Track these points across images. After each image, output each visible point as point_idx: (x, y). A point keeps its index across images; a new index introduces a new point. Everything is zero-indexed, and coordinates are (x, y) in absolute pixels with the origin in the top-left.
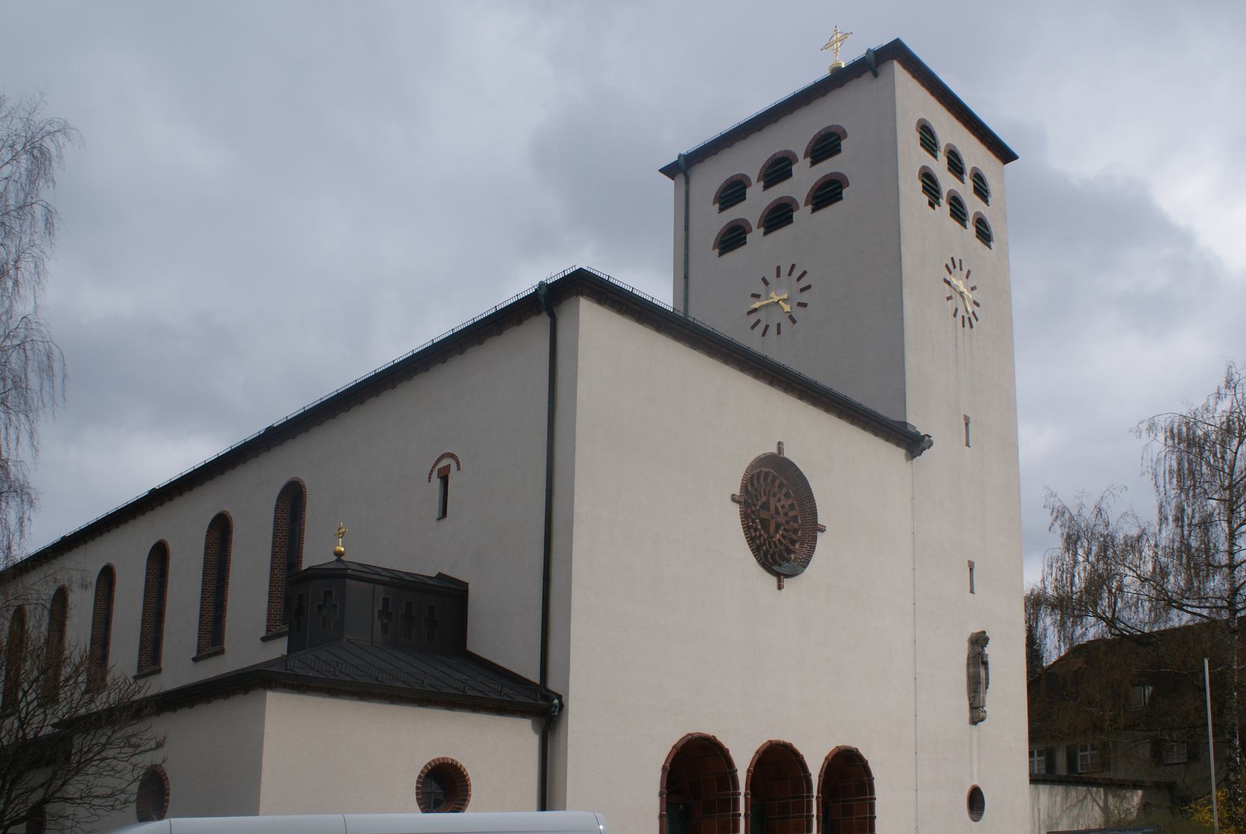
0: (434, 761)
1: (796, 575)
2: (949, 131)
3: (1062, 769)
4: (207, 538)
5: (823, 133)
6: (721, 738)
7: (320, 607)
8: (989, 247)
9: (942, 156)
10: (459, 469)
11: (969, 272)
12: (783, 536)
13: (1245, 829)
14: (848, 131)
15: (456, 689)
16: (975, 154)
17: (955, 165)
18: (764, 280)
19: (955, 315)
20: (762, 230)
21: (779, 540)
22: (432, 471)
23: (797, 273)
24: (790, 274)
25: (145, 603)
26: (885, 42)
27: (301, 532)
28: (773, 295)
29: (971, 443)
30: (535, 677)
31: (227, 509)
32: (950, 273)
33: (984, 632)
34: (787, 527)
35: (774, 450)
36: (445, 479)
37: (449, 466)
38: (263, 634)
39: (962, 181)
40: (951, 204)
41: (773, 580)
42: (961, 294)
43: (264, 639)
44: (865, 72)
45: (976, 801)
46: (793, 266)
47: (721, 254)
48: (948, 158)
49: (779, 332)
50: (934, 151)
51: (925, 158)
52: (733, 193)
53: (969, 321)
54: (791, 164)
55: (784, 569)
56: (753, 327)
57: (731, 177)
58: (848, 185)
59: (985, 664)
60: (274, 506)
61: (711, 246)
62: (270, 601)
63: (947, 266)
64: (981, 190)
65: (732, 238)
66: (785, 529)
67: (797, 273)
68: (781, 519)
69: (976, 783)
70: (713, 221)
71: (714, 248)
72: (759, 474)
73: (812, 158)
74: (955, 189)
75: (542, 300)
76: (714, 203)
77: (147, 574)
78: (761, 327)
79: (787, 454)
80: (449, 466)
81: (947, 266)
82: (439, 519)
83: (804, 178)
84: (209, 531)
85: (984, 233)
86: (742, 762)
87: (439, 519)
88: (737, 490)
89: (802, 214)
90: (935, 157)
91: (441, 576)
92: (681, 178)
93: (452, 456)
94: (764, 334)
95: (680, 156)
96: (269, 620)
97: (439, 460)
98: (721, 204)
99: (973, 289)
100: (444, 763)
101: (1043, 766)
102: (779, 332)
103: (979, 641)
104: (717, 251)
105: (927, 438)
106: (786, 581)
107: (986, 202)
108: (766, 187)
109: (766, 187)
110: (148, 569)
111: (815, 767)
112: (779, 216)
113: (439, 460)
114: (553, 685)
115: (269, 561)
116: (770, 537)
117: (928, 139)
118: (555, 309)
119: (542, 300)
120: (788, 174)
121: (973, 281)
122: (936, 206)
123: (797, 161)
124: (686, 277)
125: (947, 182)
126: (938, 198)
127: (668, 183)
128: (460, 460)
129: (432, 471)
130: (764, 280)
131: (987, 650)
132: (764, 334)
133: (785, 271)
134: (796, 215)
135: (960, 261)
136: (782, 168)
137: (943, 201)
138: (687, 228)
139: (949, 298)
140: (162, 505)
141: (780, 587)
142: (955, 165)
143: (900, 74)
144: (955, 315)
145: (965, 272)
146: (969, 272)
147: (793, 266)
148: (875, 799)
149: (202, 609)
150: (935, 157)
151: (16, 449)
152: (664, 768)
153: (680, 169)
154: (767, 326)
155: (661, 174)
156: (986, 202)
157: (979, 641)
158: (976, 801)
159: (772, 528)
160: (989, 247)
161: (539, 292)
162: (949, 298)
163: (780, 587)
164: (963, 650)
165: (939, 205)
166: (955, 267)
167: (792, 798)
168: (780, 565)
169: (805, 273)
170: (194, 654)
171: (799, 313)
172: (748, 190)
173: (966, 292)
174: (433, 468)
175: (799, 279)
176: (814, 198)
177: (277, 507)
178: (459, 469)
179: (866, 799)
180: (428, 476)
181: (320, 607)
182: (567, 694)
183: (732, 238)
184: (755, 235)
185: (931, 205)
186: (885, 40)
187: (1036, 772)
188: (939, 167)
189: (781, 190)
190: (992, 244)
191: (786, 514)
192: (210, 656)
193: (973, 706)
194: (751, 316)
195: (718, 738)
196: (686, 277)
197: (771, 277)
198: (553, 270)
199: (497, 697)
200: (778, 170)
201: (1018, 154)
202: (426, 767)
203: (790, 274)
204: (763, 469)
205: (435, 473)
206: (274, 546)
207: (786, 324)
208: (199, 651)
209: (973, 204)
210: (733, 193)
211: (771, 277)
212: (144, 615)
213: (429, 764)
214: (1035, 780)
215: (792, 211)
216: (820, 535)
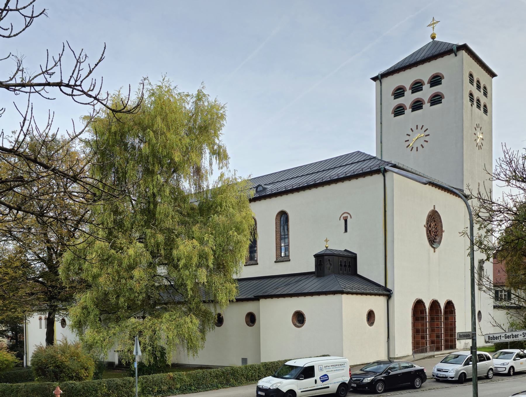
13: (59, 396)
16: (479, 74)
18: (411, 129)
20: (411, 110)
22: (341, 217)
23: (424, 129)
24: (421, 129)
36: (346, 221)
46: (423, 126)
50: (472, 82)
52: (399, 92)
54: (422, 85)
57: (416, 80)
65: (399, 111)
67: (424, 129)
71: (392, 113)
73: (431, 84)
83: (427, 93)
89: (427, 105)
91: (346, 250)
92: (378, 81)
97: (343, 214)
104: (393, 115)
108: (413, 93)
109: (413, 93)
112: (417, 105)
113: (343, 214)
114: (389, 287)
127: (374, 83)
129: (341, 217)
130: (411, 129)
143: (463, 53)
147: (423, 126)
148: (455, 316)
161: (381, 169)
174: (341, 216)
175: (425, 131)
182: (394, 290)
183: (399, 111)
186: (461, 43)
189: (418, 95)
190: (488, 114)
197: (414, 128)
205: (342, 218)
206: (276, 232)
209: (483, 100)
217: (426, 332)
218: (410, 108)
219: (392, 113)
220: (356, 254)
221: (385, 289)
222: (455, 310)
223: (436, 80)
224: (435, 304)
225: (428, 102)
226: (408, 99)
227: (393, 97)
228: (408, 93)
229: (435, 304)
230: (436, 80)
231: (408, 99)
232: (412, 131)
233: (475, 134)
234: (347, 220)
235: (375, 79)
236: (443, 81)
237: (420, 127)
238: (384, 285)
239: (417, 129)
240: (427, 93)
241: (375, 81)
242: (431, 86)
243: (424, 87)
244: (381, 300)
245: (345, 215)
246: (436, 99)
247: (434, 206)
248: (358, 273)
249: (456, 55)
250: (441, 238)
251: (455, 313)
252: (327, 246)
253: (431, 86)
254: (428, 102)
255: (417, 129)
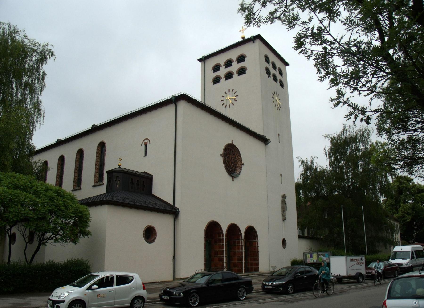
0: (148, 226)
1: (237, 177)
2: (272, 58)
3: (306, 235)
4: (76, 155)
5: (240, 55)
6: (219, 222)
7: (115, 180)
8: (283, 88)
9: (271, 64)
10: (150, 143)
11: (278, 95)
12: (233, 166)
14: (247, 56)
15: (153, 206)
16: (279, 64)
17: (274, 67)
18: (225, 92)
19: (275, 106)
21: (232, 167)
23: (234, 92)
24: (232, 92)
25: (57, 173)
26: (256, 34)
27: (104, 157)
28: (228, 96)
29: (280, 142)
30: (172, 204)
31: (82, 148)
32: (274, 95)
33: (285, 195)
34: (234, 163)
35: (231, 142)
36: (146, 146)
37: (147, 142)
38: (93, 185)
39: (276, 70)
40: (273, 77)
41: (231, 178)
42: (277, 101)
43: (93, 186)
44: (251, 41)
45: (284, 242)
46: (233, 90)
47: (214, 84)
48: (272, 65)
49: (229, 107)
51: (266, 65)
52: (216, 68)
53: (279, 108)
54: (232, 62)
55: (234, 175)
56: (223, 105)
58: (247, 70)
59: (285, 204)
60: (96, 148)
61: (211, 81)
62: (95, 175)
63: (273, 93)
64: (281, 73)
65: (217, 80)
66: (234, 164)
67: (234, 92)
68: (233, 161)
69: (284, 237)
70: (212, 75)
71: (212, 82)
72: (227, 148)
74: (274, 73)
75: (173, 100)
76: (212, 70)
77: (58, 164)
78: (225, 105)
79: (235, 143)
80: (147, 142)
81: (273, 93)
82: (144, 156)
83: (235, 67)
84: (77, 154)
85: (282, 85)
86: (225, 229)
87: (144, 156)
88: (222, 153)
89: (235, 76)
90: (269, 64)
91: (145, 172)
93: (148, 139)
94: (225, 107)
95: (203, 57)
96: (95, 181)
97: (144, 140)
98: (214, 71)
99: (280, 99)
100: (150, 227)
101: (301, 232)
102: (229, 107)
103: (284, 197)
104: (213, 83)
105: (269, 140)
106: (235, 179)
107: (282, 76)
108: (226, 68)
109: (226, 68)
110: (58, 163)
111: (243, 231)
112: (229, 76)
113: (144, 140)
114: (177, 206)
115: (95, 164)
116: (230, 166)
117: (267, 59)
118: (176, 103)
119: (173, 100)
120: (231, 65)
121: (279, 97)
122: (270, 77)
123: (234, 62)
124: (204, 89)
125: (272, 71)
126: (270, 75)
127: (199, 63)
128: (150, 141)
130: (225, 92)
131: (286, 200)
132: (225, 107)
133: (231, 91)
134: (233, 76)
135: (276, 92)
136: (230, 63)
137: (271, 76)
138: (204, 76)
139: (274, 102)
140: (63, 145)
141: (233, 180)
142: (274, 67)
143: (258, 41)
144: (275, 106)
145: (277, 95)
146: (278, 95)
147: (233, 90)
148: (258, 241)
149: (74, 176)
150: (269, 64)
151: (354, 289)
152: (205, 230)
153: (203, 60)
154: (226, 105)
155: (198, 61)
156: (282, 76)
157: (284, 197)
158: (284, 242)
159: (230, 164)
160: (283, 88)
161: (173, 98)
162: (274, 102)
163: (233, 180)
164: (280, 199)
165: (270, 77)
166: (275, 94)
167: (237, 240)
168: (233, 174)
169: (236, 92)
170: (72, 189)
171: (235, 102)
172: (221, 68)
173: (278, 100)
174: (143, 142)
175: (235, 93)
176: (238, 72)
177: (97, 148)
178: (150, 143)
179: (256, 241)
180: (141, 144)
181: (115, 180)
183: (217, 80)
184: (223, 80)
185: (268, 77)
187: (299, 235)
188: (270, 67)
189: (229, 69)
191: (234, 160)
192: (77, 190)
193: (283, 215)
194: (222, 102)
195: (218, 222)
196: (204, 89)
198: (176, 92)
199: (163, 208)
200: (229, 63)
201: (290, 64)
202: (146, 227)
203: (232, 92)
204: (228, 147)
205: (143, 143)
206: (96, 160)
207: (231, 105)
208: (73, 188)
209: (279, 77)
210: (216, 68)
211: (227, 92)
212: (57, 176)
213: (147, 227)
214: (299, 237)
215: (232, 75)
216: (243, 166)
217: (223, 254)
218: (224, 78)
219: (212, 82)
220: (152, 175)
221: (173, 207)
222: (257, 236)
223: (241, 59)
224: (233, 228)
225: (236, 73)
226: (223, 71)
227: (213, 71)
228: (223, 68)
229: (233, 228)
230: (241, 59)
231: (223, 71)
232: (226, 93)
233: (273, 98)
234: (147, 145)
235: (200, 60)
236: (246, 59)
237: (231, 91)
238: (172, 204)
239: (229, 92)
240: (235, 67)
241: (201, 62)
242: (238, 63)
243: (233, 64)
244: (168, 220)
245: (146, 141)
246: (242, 71)
247: (232, 140)
248: (153, 193)
249: (254, 42)
250: (241, 169)
251: (257, 239)
252: (120, 164)
253: (238, 63)
254: (236, 73)
255: (229, 92)
